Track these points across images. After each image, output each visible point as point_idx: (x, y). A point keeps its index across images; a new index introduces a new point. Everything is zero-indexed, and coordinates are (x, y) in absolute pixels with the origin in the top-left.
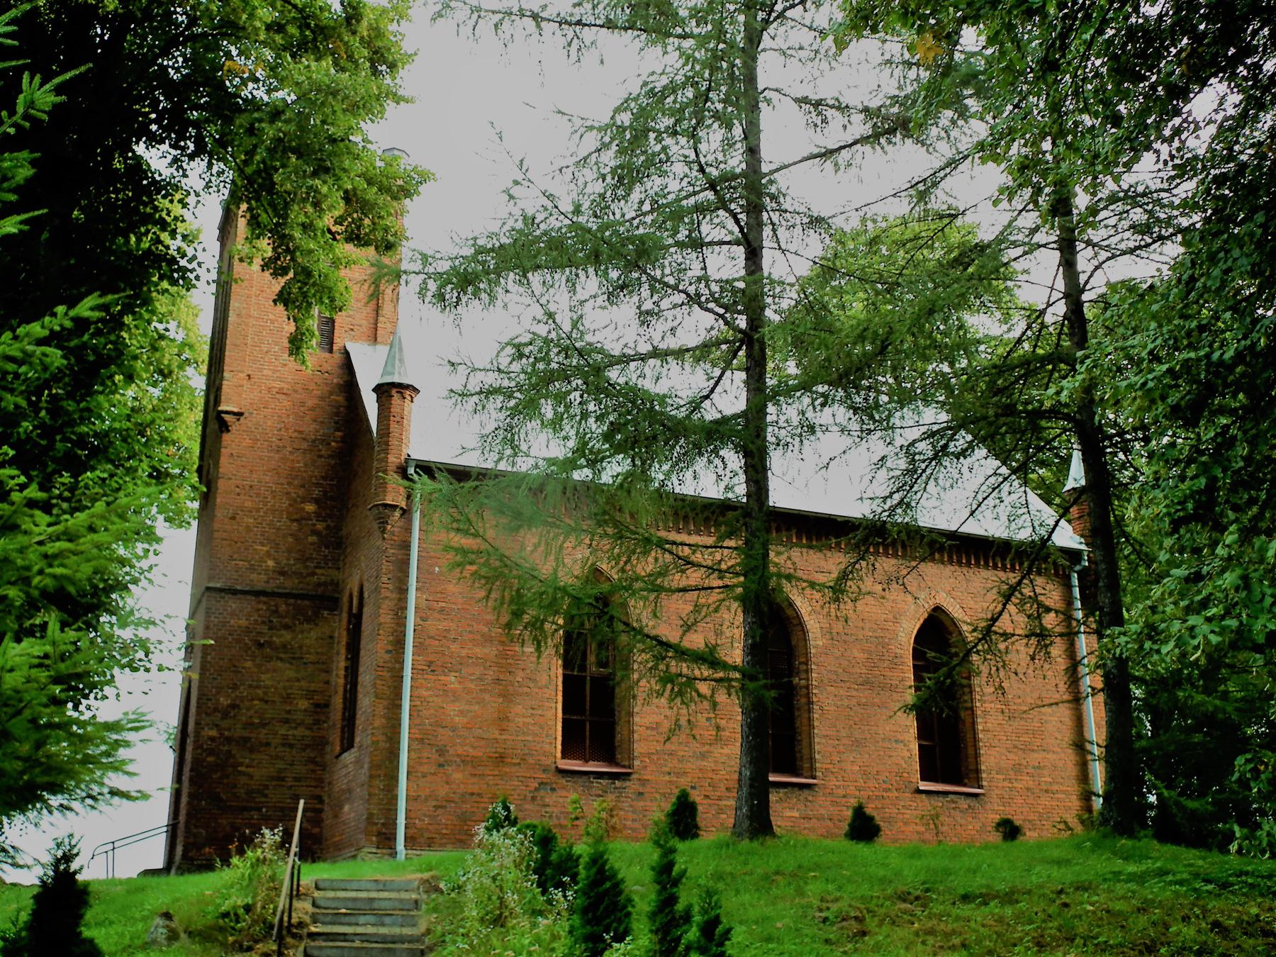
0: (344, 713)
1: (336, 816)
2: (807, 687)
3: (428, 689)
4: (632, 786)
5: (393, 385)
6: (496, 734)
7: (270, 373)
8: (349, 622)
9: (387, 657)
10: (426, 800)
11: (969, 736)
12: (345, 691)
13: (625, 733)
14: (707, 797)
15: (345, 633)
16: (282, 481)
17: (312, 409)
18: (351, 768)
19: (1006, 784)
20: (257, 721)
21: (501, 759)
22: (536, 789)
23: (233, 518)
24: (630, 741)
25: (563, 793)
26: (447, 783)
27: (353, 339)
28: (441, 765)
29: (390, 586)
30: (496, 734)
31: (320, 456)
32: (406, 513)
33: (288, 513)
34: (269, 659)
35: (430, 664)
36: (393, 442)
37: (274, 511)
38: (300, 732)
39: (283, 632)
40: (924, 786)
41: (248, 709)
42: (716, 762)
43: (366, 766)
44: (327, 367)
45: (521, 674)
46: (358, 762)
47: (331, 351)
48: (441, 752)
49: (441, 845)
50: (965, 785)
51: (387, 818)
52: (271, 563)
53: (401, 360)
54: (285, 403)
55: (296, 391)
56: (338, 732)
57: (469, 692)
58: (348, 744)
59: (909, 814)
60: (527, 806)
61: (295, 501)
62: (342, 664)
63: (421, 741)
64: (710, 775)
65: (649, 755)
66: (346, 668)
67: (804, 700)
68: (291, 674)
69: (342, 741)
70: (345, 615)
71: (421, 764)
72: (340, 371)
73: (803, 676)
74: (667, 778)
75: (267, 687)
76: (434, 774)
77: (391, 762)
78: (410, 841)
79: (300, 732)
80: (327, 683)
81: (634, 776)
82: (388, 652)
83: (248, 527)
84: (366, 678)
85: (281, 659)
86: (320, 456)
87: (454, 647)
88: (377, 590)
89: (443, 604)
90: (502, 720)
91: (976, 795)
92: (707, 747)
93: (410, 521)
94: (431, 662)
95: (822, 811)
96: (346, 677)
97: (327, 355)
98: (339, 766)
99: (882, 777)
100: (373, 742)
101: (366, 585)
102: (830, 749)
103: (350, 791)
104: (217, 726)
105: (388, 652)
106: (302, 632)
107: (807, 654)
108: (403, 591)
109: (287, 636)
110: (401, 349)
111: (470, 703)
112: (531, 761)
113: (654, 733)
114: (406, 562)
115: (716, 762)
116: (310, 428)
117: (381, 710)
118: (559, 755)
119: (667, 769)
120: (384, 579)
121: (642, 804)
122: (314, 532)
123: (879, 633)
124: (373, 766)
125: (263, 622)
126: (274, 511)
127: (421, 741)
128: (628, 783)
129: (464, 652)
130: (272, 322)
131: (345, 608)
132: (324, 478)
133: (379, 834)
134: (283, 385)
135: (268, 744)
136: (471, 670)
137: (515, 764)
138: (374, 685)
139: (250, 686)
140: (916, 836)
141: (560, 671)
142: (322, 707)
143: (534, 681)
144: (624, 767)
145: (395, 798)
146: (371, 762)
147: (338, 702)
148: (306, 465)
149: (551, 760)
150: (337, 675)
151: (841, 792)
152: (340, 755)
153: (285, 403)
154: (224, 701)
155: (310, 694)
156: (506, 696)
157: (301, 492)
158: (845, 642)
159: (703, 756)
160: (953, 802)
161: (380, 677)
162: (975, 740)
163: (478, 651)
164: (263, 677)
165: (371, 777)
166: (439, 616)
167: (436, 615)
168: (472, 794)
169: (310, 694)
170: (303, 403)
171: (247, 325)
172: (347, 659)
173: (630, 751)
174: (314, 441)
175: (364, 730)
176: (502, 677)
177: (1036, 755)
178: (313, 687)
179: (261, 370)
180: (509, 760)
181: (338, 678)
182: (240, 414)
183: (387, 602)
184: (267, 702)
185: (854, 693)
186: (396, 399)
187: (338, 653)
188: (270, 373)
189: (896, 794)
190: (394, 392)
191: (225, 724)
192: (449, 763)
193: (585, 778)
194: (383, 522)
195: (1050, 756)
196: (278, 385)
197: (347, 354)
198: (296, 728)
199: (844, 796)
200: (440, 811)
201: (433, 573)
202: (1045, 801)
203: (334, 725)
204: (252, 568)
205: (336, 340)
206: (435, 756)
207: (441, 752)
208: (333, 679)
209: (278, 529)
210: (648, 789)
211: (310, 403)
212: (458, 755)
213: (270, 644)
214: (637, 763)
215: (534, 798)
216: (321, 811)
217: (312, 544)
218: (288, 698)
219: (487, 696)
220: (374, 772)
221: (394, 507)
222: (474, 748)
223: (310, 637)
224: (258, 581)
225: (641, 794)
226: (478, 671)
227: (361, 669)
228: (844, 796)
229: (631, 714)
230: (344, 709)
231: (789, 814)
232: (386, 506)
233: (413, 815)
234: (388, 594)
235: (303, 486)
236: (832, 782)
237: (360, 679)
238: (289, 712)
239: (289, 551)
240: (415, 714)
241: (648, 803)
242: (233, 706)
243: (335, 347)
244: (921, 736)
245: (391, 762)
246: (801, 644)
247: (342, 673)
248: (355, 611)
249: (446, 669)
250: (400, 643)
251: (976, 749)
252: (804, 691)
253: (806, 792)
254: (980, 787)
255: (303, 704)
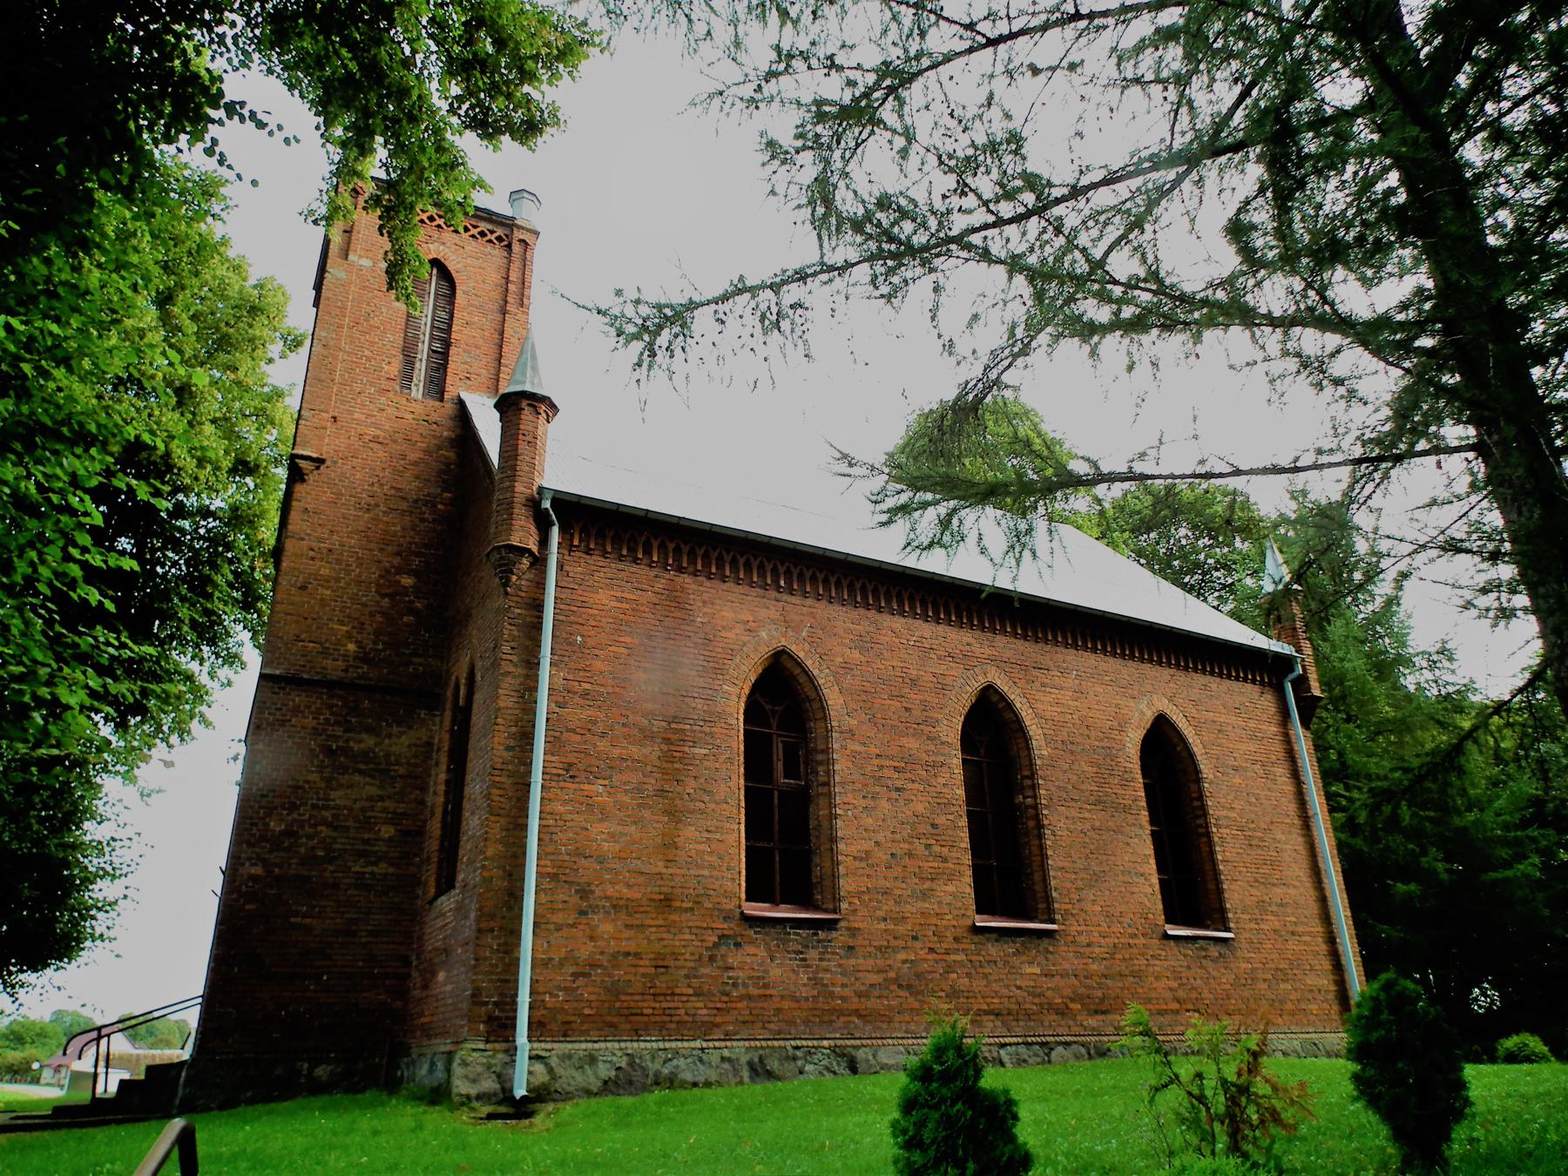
0: (442, 843)
1: (426, 987)
2: (1035, 807)
3: (565, 802)
4: (839, 937)
5: (524, 395)
6: (660, 866)
7: (363, 417)
8: (453, 722)
9: (507, 755)
10: (562, 963)
11: (1208, 867)
12: (445, 812)
13: (827, 864)
14: (932, 950)
15: (447, 736)
16: (372, 546)
17: (415, 464)
18: (450, 917)
19: (1253, 925)
20: (321, 853)
21: (666, 902)
22: (716, 945)
23: (303, 588)
24: (834, 877)
25: (752, 950)
26: (592, 938)
27: (469, 389)
28: (583, 913)
29: (514, 658)
30: (660, 866)
31: (423, 520)
32: (539, 562)
33: (378, 585)
34: (344, 770)
35: (569, 767)
36: (523, 467)
37: (359, 583)
38: (382, 868)
39: (364, 736)
40: (1174, 931)
41: (310, 837)
42: (940, 903)
43: (473, 915)
44: (434, 417)
45: (692, 783)
46: (460, 909)
47: (442, 400)
48: (584, 893)
49: (582, 1033)
50: (1207, 928)
51: (502, 995)
52: (351, 647)
53: (535, 369)
54: (381, 454)
55: (395, 442)
56: (433, 868)
57: (622, 806)
58: (446, 882)
59: (1159, 966)
60: (703, 971)
61: (388, 572)
62: (443, 777)
63: (554, 877)
64: (934, 920)
65: (859, 894)
66: (447, 782)
67: (1031, 824)
68: (373, 791)
69: (438, 881)
70: (448, 714)
71: (553, 911)
72: (450, 423)
73: (1029, 793)
74: (882, 926)
75: (337, 807)
76: (573, 926)
77: (510, 909)
78: (538, 1028)
79: (382, 868)
80: (422, 802)
81: (842, 924)
82: (509, 748)
83: (322, 600)
84: (475, 788)
85: (361, 772)
86: (423, 520)
87: (602, 745)
88: (495, 664)
89: (587, 686)
90: (669, 846)
91: (1225, 940)
92: (927, 885)
93: (543, 574)
94: (570, 765)
95: (1067, 966)
96: (447, 793)
97: (437, 404)
98: (433, 915)
99: (1126, 920)
100: (484, 880)
101: (479, 664)
102: (1069, 885)
103: (446, 951)
104: (263, 861)
105: (509, 748)
106: (390, 736)
107: (1031, 765)
108: (532, 664)
109: (369, 741)
110: (534, 357)
111: (622, 823)
112: (708, 905)
113: (863, 864)
114: (537, 626)
115: (940, 903)
116: (410, 485)
117: (496, 831)
118: (743, 896)
119: (881, 913)
120: (506, 649)
121: (853, 961)
122: (412, 611)
123: (1106, 743)
124: (483, 914)
125: (337, 723)
126: (359, 583)
127: (554, 877)
128: (834, 934)
129: (616, 752)
130: (369, 359)
131: (448, 706)
132: (425, 546)
133: (490, 1019)
134: (378, 432)
135: (335, 886)
136: (624, 777)
137: (686, 910)
138: (488, 796)
139: (314, 806)
140: (1169, 995)
141: (742, 781)
142: (412, 835)
143: (709, 793)
144: (826, 911)
145: (515, 964)
146: (480, 909)
147: (435, 827)
148: (403, 529)
149: (735, 902)
150: (435, 793)
151: (1083, 939)
152: (436, 898)
153: (381, 454)
154: (275, 826)
155: (395, 819)
156: (675, 815)
157: (397, 561)
158: (1072, 752)
159: (924, 895)
160: (1202, 948)
161: (494, 784)
162: (1216, 873)
163: (634, 750)
164: (333, 794)
165: (479, 931)
166: (581, 702)
167: (577, 699)
168: (628, 954)
169: (395, 819)
170: (403, 457)
171: (335, 358)
172: (449, 770)
173: (835, 887)
174: (416, 501)
175: (471, 862)
176: (667, 787)
177: (1277, 890)
178: (402, 808)
179: (350, 413)
180: (678, 904)
181: (437, 797)
182: (319, 462)
183: (509, 679)
184: (336, 828)
185: (1087, 815)
186: (527, 414)
187: (437, 764)
188: (363, 417)
189: (1142, 940)
190: (524, 404)
191: (273, 857)
192: (594, 909)
193: (779, 929)
194: (505, 571)
195: (1292, 891)
196: (372, 431)
197: (461, 404)
198: (376, 864)
199: (1088, 945)
200: (581, 981)
201: (574, 643)
202: (1292, 945)
203: (428, 858)
204: (325, 653)
205: (448, 388)
206: (575, 900)
207: (584, 893)
208: (429, 800)
209: (364, 605)
210: (859, 941)
211: (413, 456)
212: (608, 898)
213: (345, 751)
214: (844, 905)
215: (712, 958)
216: (408, 976)
217: (407, 625)
218: (366, 824)
219: (647, 814)
220: (483, 925)
221: (523, 551)
222: (629, 886)
223: (401, 743)
224: (334, 668)
225: (851, 948)
226: (635, 778)
227: (469, 778)
228: (1088, 945)
229: (833, 840)
230: (443, 836)
231: (1029, 970)
232: (511, 548)
233: (541, 989)
234: (511, 668)
235: (399, 554)
236: (1074, 928)
237: (467, 791)
238: (366, 842)
239: (377, 633)
240: (547, 838)
241: (861, 961)
242: (288, 833)
243: (446, 396)
244: (1160, 871)
245: (510, 909)
246: (1023, 754)
247: (442, 788)
248: (461, 703)
249: (593, 775)
250: (527, 737)
251: (1218, 883)
252: (1031, 812)
253: (1046, 942)
254: (1228, 930)
255: (387, 831)
